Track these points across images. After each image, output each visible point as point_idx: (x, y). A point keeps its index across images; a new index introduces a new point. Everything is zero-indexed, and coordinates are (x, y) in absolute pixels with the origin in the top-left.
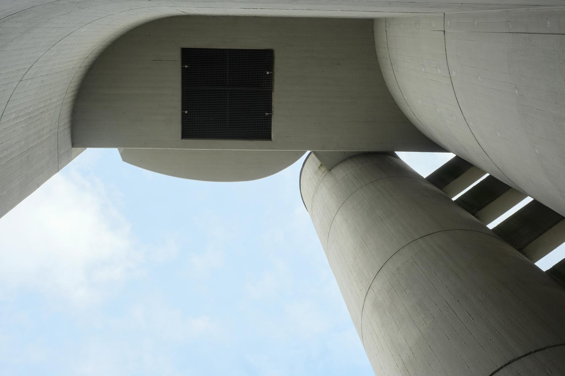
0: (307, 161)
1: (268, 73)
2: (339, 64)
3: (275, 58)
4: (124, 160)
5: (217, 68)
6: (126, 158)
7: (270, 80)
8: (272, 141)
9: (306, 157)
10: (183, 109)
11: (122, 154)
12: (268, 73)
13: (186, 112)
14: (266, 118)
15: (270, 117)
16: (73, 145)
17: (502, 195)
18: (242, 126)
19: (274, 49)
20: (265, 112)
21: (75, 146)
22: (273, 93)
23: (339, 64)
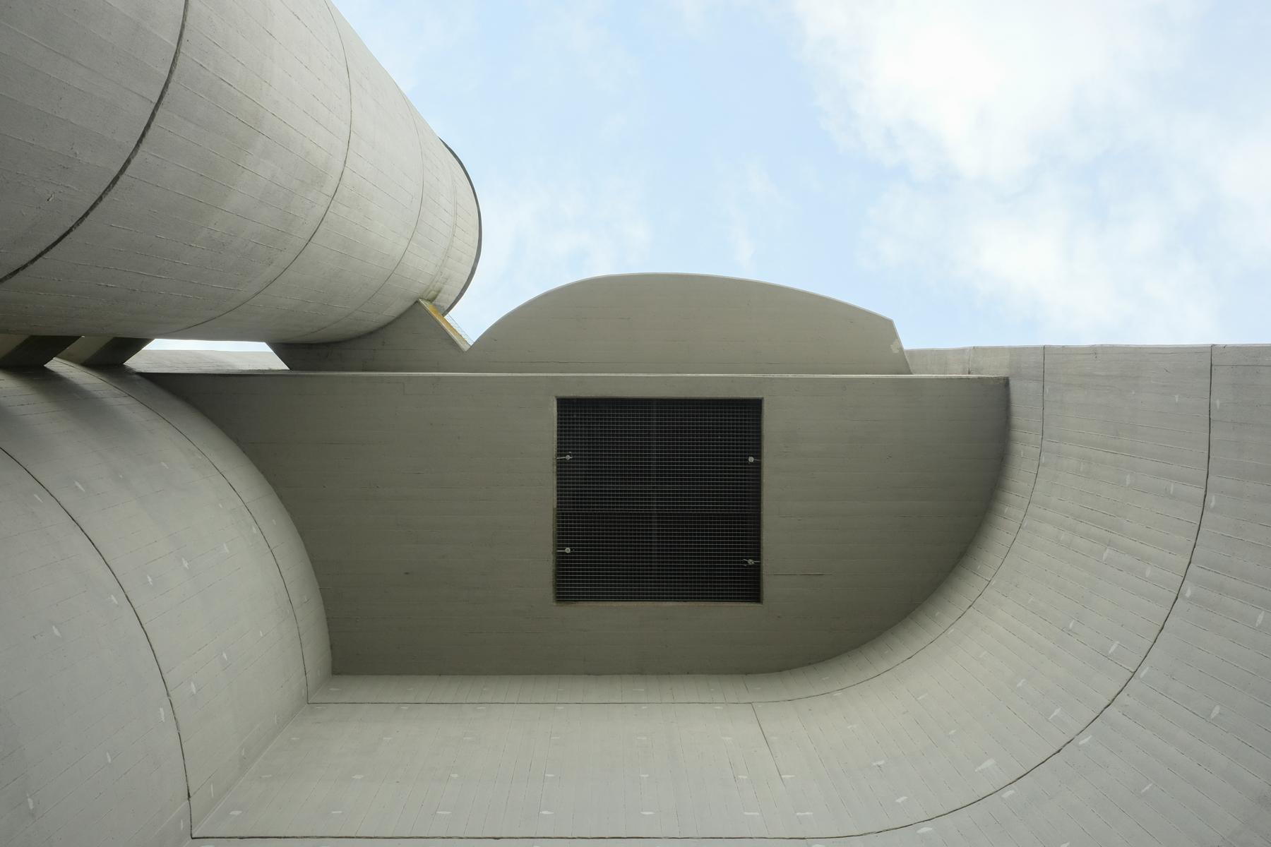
0: (469, 273)
1: (568, 550)
2: (407, 573)
3: (551, 584)
4: (888, 324)
5: (673, 499)
6: (886, 328)
7: (563, 533)
8: (556, 397)
9: (471, 284)
10: (758, 466)
11: (894, 336)
12: (568, 550)
13: (751, 459)
14: (569, 447)
15: (561, 450)
16: (1006, 383)
17: (17, 346)
18: (629, 428)
19: (555, 604)
20: (573, 459)
21: (1002, 381)
22: (555, 507)
23: (407, 573)
